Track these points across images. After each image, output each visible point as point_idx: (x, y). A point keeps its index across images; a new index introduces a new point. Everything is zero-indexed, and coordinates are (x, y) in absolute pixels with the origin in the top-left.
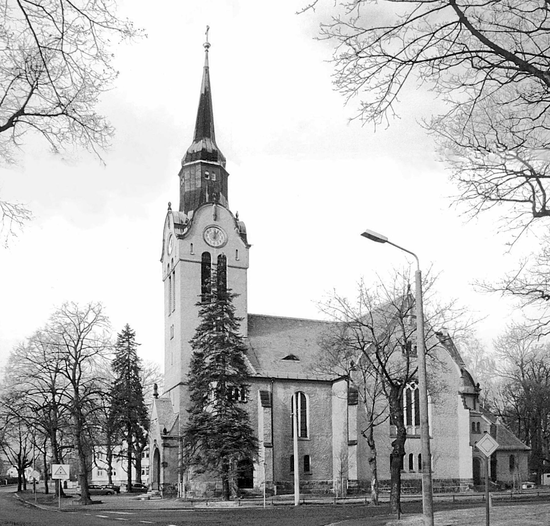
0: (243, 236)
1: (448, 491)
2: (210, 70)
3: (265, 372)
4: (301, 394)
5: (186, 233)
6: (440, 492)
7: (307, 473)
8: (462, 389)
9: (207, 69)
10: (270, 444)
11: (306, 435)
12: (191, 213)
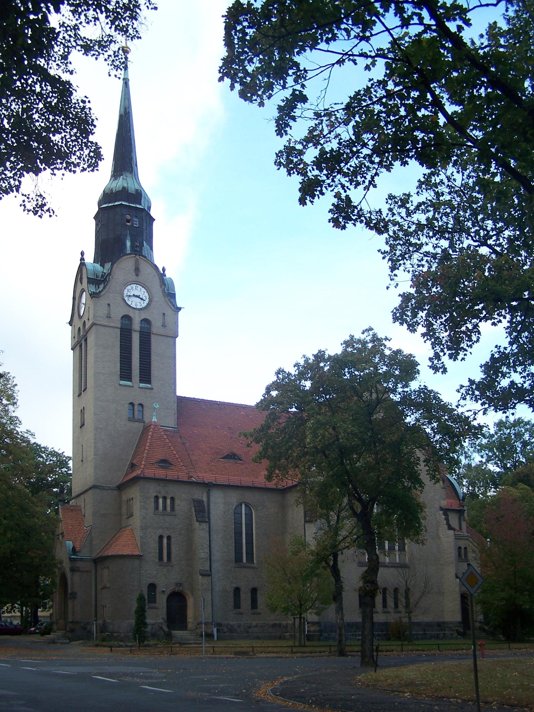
0: (172, 296)
1: (431, 637)
3: (200, 475)
5: (102, 290)
6: (422, 639)
7: (254, 611)
8: (444, 503)
10: (207, 570)
11: (253, 560)
12: (108, 265)
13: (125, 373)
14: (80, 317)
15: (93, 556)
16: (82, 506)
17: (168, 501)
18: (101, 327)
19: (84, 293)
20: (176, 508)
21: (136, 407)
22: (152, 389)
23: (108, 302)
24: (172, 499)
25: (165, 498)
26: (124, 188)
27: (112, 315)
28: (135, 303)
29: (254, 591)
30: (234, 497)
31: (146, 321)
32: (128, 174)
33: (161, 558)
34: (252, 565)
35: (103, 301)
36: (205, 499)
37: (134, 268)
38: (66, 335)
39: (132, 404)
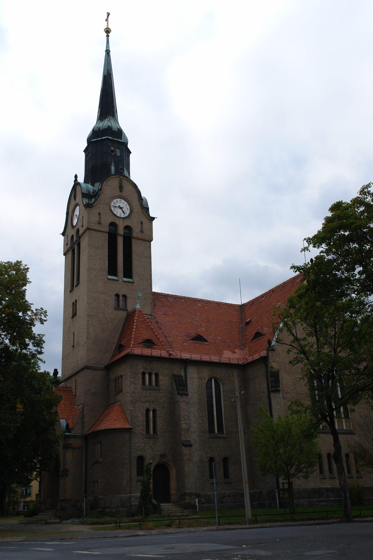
0: (147, 209)
2: (111, 54)
4: (215, 380)
9: (108, 52)
11: (223, 431)
13: (112, 270)
14: (73, 227)
15: (85, 432)
16: (73, 387)
17: (153, 377)
18: (93, 232)
19: (78, 207)
20: (161, 383)
21: (121, 297)
22: (133, 283)
23: (99, 212)
24: (157, 375)
25: (150, 375)
26: (109, 127)
27: (102, 222)
28: (118, 212)
29: (225, 460)
30: (206, 373)
31: (128, 228)
32: (111, 118)
33: (148, 431)
34: (222, 435)
35: (95, 211)
36: (183, 374)
37: (118, 186)
38: (60, 242)
39: (117, 295)
